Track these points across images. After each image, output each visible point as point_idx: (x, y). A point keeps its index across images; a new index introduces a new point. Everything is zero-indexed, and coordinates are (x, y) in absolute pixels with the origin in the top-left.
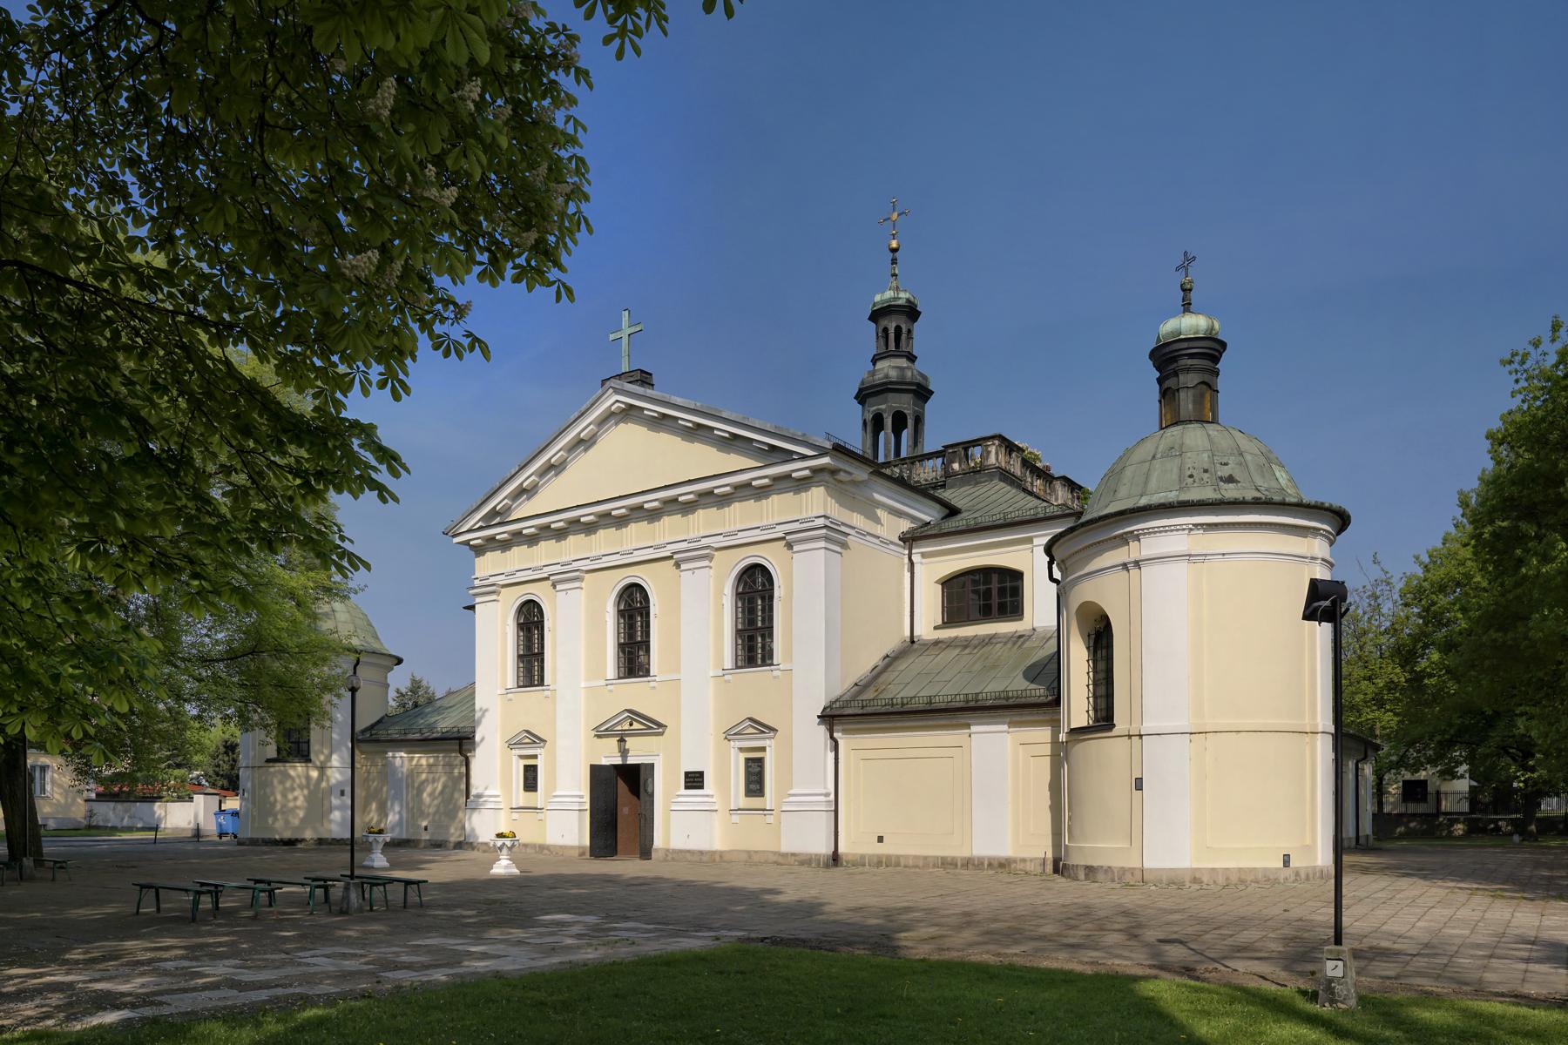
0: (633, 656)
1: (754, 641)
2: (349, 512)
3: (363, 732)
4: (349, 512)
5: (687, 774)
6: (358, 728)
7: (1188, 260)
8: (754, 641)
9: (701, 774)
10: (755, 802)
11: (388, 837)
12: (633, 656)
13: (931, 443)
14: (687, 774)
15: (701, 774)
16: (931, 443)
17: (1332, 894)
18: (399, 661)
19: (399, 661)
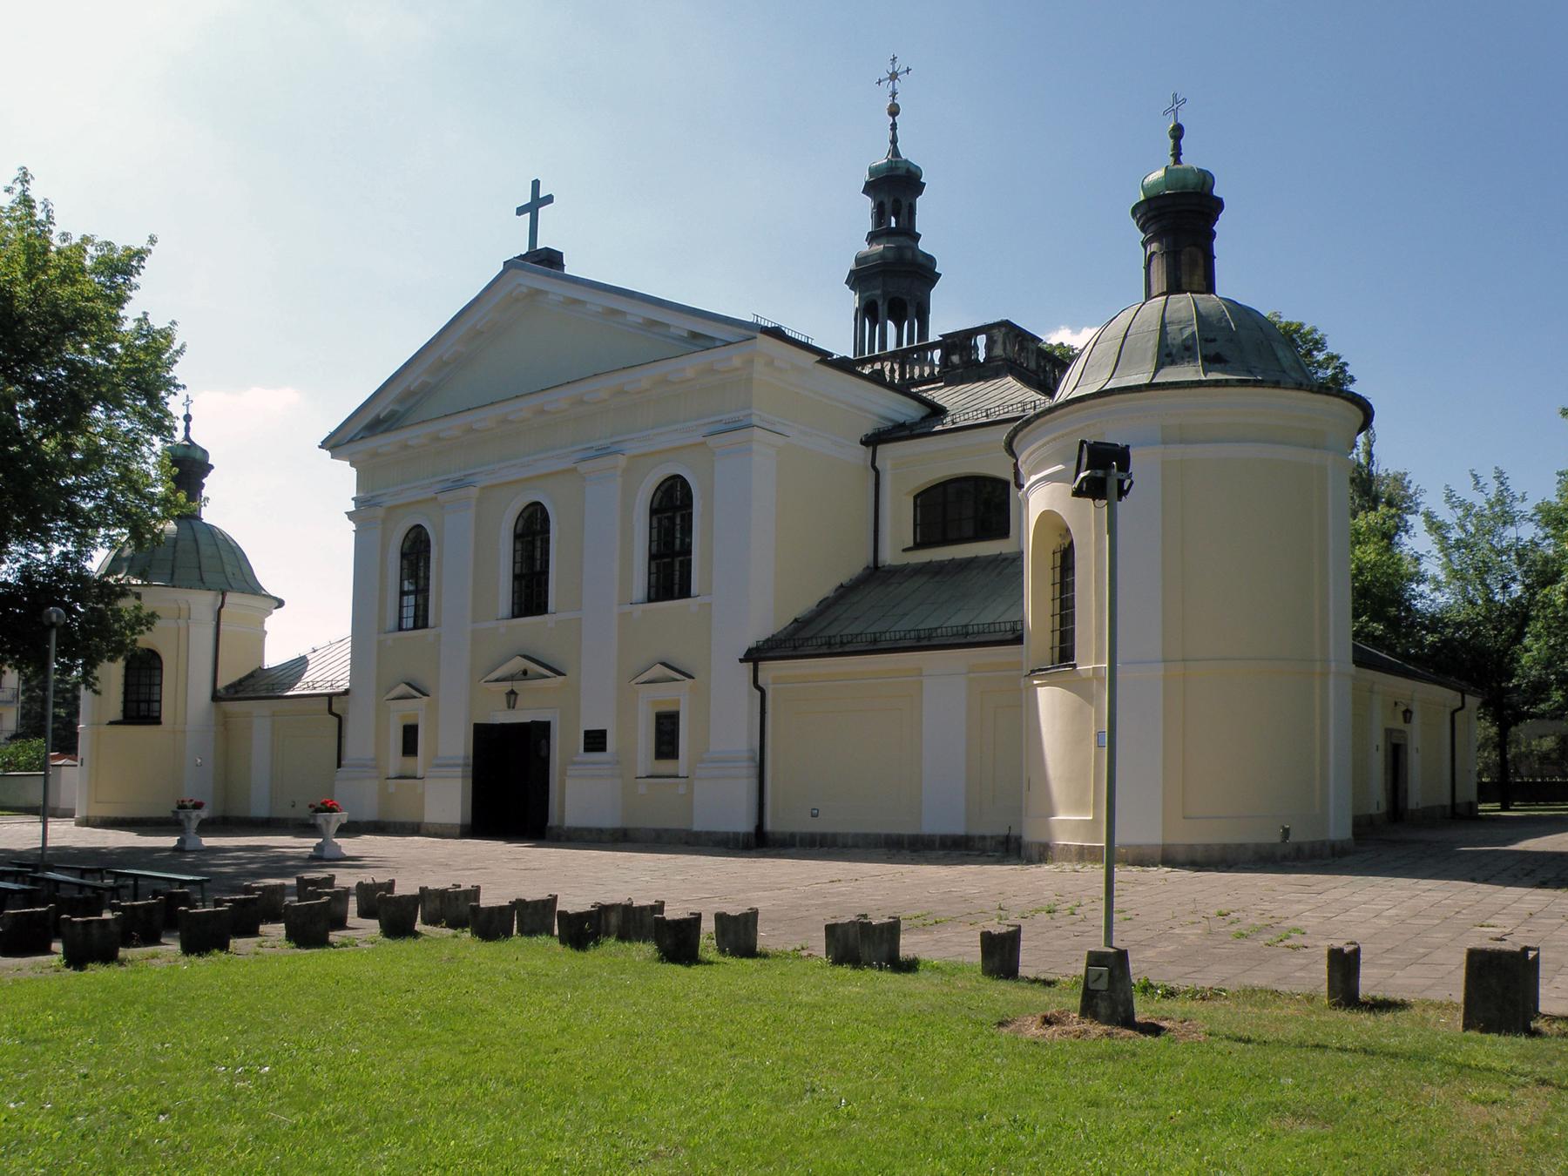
0: (531, 594)
1: (670, 573)
2: (1307, 328)
3: (228, 688)
4: (1307, 328)
5: (587, 733)
6: (221, 684)
7: (536, 203)
8: (670, 573)
9: (603, 733)
10: (666, 766)
11: (204, 814)
12: (531, 594)
13: (933, 336)
14: (587, 733)
15: (603, 733)
16: (933, 336)
17: (1103, 879)
18: (281, 603)
19: (281, 603)
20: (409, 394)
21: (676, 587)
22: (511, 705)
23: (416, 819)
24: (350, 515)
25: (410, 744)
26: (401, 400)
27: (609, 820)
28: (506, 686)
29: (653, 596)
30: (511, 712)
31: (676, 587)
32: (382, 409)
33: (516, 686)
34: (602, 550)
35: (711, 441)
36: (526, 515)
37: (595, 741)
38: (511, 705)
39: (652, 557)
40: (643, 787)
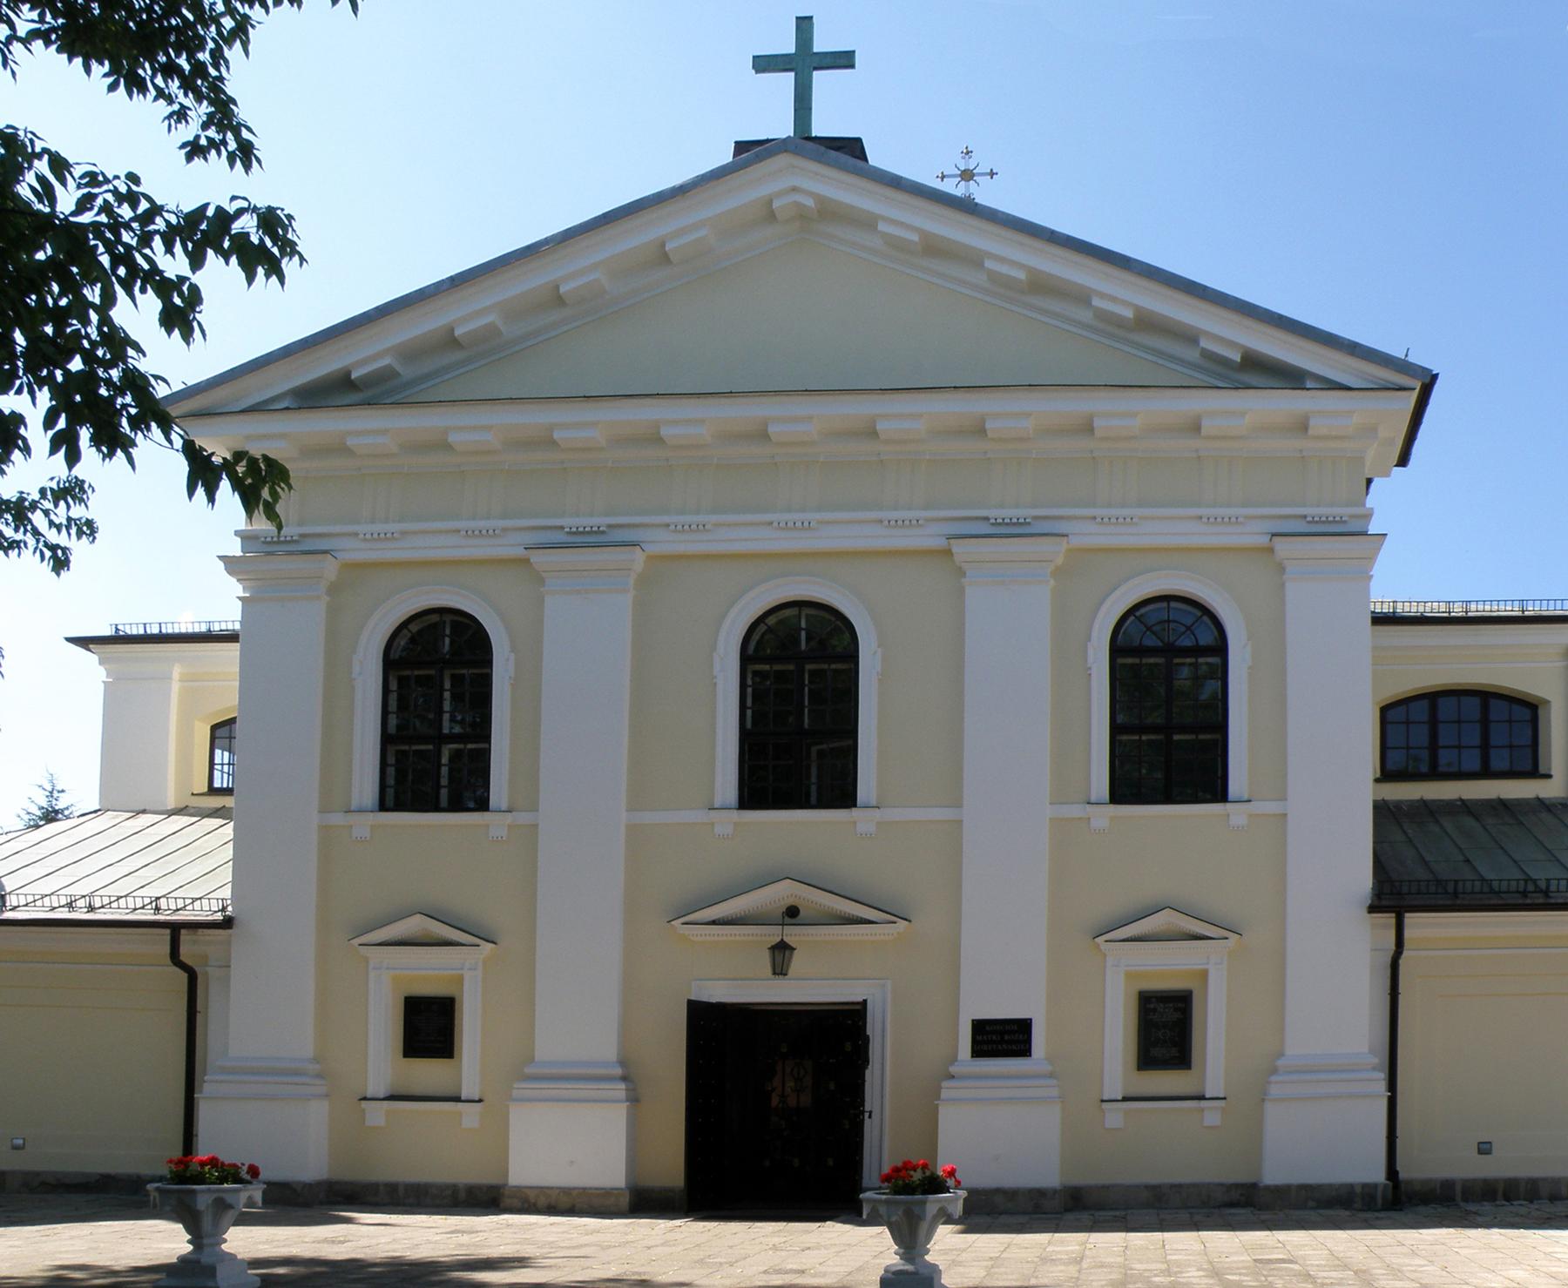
10: (428, 1073)
20: (449, 341)
21: (444, 792)
22: (780, 970)
23: (1237, 1175)
24: (230, 563)
25: (429, 1026)
26: (411, 353)
27: (1044, 1170)
28: (773, 935)
29: (390, 800)
30: (779, 981)
31: (444, 792)
32: (359, 357)
33: (792, 935)
34: (989, 710)
35: (537, 558)
36: (414, 628)
37: (1002, 1038)
38: (780, 970)
39: (386, 739)
40: (1115, 1117)
